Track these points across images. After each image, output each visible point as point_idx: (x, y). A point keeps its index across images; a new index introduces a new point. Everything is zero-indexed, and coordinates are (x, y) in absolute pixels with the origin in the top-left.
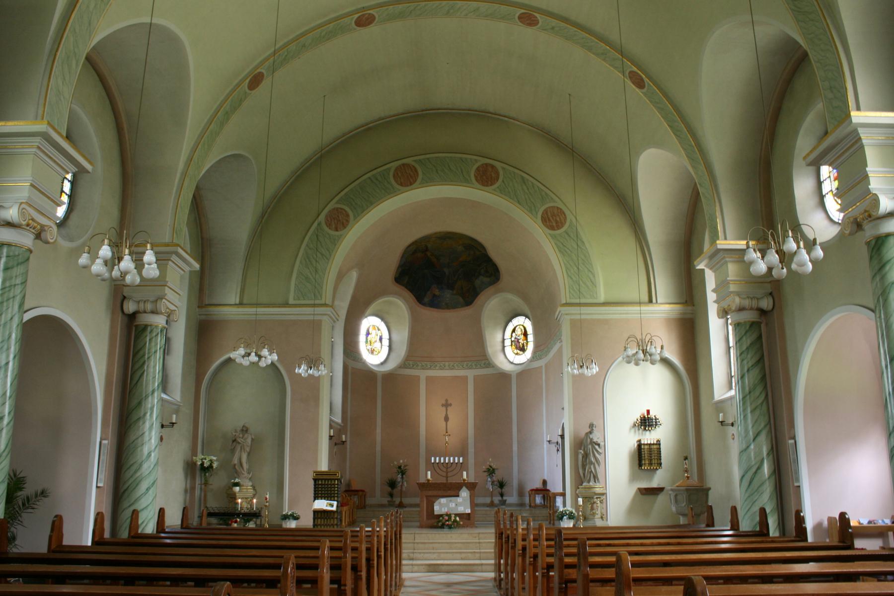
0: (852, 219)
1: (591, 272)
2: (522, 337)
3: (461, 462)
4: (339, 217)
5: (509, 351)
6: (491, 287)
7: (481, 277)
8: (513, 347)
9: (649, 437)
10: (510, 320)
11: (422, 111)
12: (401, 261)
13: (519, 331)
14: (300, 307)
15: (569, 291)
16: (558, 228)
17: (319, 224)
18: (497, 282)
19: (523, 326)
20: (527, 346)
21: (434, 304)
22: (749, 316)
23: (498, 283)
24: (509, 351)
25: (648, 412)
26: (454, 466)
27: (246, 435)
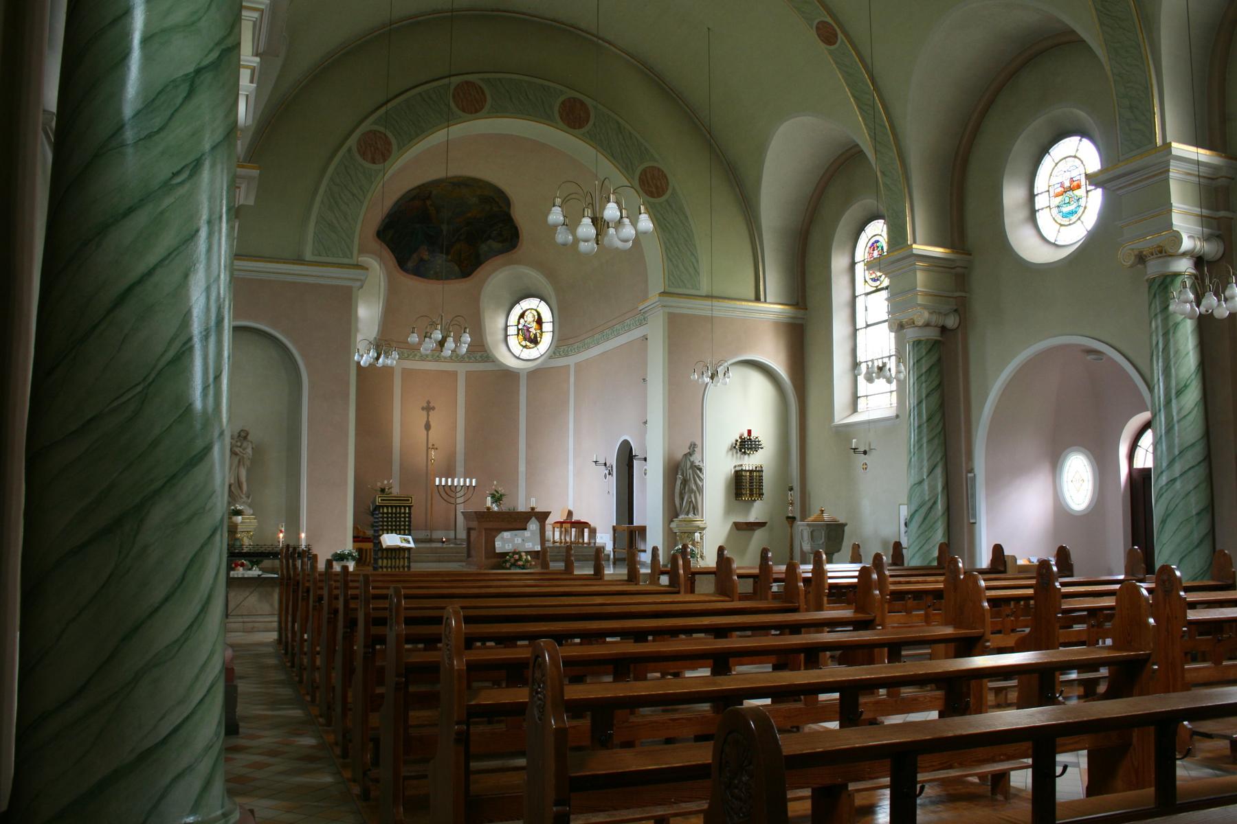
0: (1136, 252)
1: (694, 255)
2: (534, 325)
3: (474, 485)
4: (376, 143)
5: (513, 342)
6: (501, 256)
7: (490, 242)
8: (521, 337)
9: (751, 462)
10: (518, 302)
11: (492, 11)
12: (391, 210)
13: (529, 317)
14: (323, 266)
15: (669, 277)
16: (659, 195)
17: (349, 150)
18: (511, 250)
19: (536, 310)
20: (541, 338)
21: (420, 271)
22: (932, 334)
23: (513, 251)
24: (513, 342)
25: (749, 432)
26: (471, 489)
27: (245, 444)
